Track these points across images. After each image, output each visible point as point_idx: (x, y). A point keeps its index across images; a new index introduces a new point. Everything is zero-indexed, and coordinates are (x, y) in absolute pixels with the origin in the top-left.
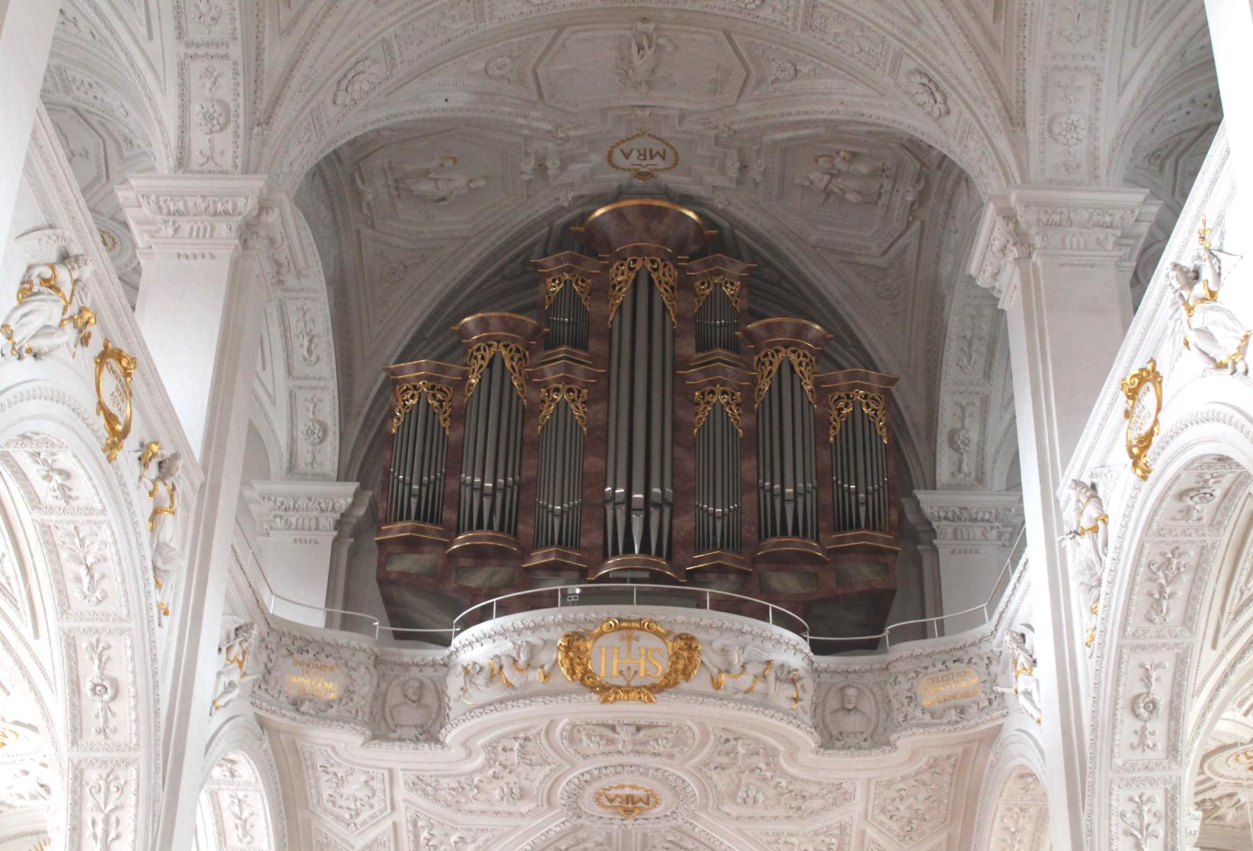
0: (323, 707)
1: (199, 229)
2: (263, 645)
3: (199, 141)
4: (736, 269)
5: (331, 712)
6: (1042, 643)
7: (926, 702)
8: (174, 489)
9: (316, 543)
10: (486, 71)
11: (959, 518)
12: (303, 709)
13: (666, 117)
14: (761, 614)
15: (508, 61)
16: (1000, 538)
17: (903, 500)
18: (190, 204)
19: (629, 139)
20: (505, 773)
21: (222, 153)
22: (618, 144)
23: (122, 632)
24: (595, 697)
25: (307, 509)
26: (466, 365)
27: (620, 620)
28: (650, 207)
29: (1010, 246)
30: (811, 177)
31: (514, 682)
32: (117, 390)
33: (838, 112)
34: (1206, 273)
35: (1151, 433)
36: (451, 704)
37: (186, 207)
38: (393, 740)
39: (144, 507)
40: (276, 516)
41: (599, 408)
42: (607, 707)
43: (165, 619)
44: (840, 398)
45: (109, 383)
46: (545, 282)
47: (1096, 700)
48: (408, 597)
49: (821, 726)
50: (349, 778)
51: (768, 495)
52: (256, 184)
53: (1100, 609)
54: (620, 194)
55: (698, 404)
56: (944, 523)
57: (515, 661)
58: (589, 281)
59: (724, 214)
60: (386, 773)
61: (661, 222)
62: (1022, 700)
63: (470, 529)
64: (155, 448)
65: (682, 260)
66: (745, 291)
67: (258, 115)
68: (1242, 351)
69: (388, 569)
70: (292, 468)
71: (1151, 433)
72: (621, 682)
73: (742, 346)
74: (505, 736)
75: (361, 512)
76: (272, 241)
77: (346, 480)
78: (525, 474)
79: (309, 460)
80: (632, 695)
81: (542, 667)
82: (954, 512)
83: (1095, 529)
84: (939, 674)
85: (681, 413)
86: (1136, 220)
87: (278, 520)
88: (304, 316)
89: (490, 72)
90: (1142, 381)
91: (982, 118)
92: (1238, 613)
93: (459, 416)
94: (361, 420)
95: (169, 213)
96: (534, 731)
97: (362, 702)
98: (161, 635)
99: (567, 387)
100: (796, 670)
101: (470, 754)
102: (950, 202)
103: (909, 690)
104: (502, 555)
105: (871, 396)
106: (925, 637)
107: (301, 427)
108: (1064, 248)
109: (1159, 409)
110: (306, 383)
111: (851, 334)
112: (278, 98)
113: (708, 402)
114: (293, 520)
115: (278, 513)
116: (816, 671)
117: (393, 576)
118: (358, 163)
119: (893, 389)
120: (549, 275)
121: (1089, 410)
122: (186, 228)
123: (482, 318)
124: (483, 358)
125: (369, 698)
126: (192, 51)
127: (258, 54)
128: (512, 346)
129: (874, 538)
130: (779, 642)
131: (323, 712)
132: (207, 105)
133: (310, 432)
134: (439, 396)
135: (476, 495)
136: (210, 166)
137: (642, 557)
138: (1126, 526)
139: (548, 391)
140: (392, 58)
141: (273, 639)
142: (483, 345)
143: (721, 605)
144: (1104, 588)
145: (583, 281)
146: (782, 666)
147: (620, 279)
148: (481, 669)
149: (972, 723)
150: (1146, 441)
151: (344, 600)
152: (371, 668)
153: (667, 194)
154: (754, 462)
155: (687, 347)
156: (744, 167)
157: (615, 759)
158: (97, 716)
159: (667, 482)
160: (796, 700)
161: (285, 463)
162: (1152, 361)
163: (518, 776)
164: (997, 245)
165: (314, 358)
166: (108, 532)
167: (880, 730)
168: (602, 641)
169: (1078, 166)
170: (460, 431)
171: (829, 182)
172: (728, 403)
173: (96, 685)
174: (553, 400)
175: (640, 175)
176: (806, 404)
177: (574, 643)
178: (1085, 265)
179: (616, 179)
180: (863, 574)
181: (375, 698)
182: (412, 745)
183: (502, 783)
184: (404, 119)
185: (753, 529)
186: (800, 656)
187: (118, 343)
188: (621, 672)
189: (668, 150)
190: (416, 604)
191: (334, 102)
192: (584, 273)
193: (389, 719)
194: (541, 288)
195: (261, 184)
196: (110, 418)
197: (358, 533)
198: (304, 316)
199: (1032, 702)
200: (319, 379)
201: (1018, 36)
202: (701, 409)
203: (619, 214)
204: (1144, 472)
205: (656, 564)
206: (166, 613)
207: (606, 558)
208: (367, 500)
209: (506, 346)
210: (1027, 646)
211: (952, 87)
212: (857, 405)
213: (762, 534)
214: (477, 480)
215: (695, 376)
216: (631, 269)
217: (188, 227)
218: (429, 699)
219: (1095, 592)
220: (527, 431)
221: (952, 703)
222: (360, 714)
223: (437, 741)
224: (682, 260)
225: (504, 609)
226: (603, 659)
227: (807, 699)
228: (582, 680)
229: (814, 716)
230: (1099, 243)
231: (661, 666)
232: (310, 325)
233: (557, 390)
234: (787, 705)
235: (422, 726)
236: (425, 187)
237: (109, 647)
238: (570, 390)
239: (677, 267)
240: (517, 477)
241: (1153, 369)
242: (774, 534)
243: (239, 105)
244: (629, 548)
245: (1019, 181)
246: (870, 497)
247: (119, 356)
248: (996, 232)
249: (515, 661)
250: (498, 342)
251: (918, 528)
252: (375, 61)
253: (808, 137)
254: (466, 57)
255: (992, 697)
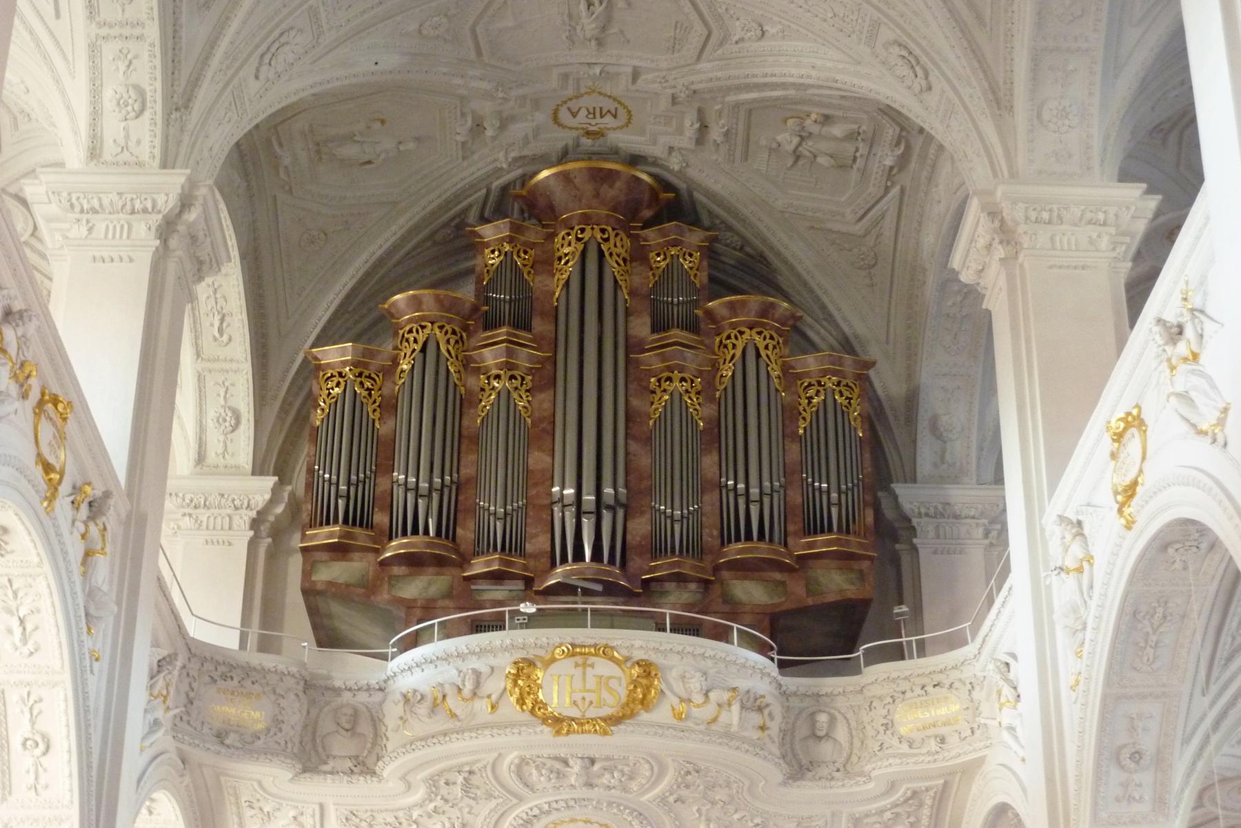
0: (249, 739)
1: (115, 227)
2: (185, 672)
3: (112, 127)
4: (695, 238)
5: (259, 743)
6: (1026, 672)
7: (903, 730)
8: (105, 529)
9: (230, 544)
10: (420, 32)
11: (942, 515)
12: (227, 742)
13: (618, 74)
14: (721, 634)
15: (444, 20)
16: (986, 535)
17: (880, 494)
18: (106, 202)
19: (577, 97)
20: (447, 808)
21: (139, 142)
22: (565, 102)
23: (55, 685)
24: (547, 729)
25: (219, 507)
26: (396, 348)
27: (574, 646)
28: (601, 170)
29: (996, 243)
30: (779, 138)
31: (458, 712)
32: (54, 437)
33: (809, 77)
34: (1189, 332)
35: (1135, 483)
36: (389, 734)
37: (101, 205)
38: (325, 773)
39: (76, 550)
40: (184, 515)
41: (544, 397)
42: (562, 739)
43: (96, 665)
44: (810, 385)
45: (46, 431)
46: (483, 253)
47: (1080, 749)
48: (336, 608)
49: (790, 756)
50: (277, 814)
51: (731, 496)
52: (176, 180)
53: (1085, 653)
54: (564, 156)
55: (653, 392)
56: (924, 520)
57: (460, 690)
58: (532, 252)
59: (681, 174)
60: (317, 808)
61: (611, 186)
62: (1006, 736)
63: (404, 534)
64: (88, 489)
65: (635, 228)
66: (705, 263)
67: (175, 99)
68: (1221, 422)
69: (313, 578)
70: (201, 459)
71: (1135, 483)
72: (575, 713)
73: (703, 326)
74: (449, 770)
75: (280, 509)
76: (193, 239)
77: (262, 473)
78: (463, 472)
79: (220, 451)
80: (586, 727)
81: (489, 696)
82: (936, 507)
83: (1080, 570)
84: (918, 700)
85: (635, 402)
86: (1133, 217)
87: (187, 518)
88: (215, 291)
89: (425, 32)
90: (1128, 426)
91: (966, 98)
92: (1229, 659)
93: (389, 407)
94: (277, 404)
95: (82, 211)
96: (480, 765)
97: (292, 733)
98: (92, 681)
99: (510, 373)
100: (763, 697)
101: (409, 786)
102: (934, 167)
103: (885, 717)
104: (440, 562)
105: (844, 383)
106: (903, 658)
107: (211, 414)
108: (1054, 249)
109: (1144, 458)
110: (217, 366)
111: (823, 307)
112: (197, 79)
113: (665, 391)
114: (205, 519)
115: (187, 511)
116: (785, 695)
117: (319, 587)
118: (275, 127)
119: (872, 373)
120: (487, 245)
121: (1079, 432)
122: (100, 227)
123: (414, 296)
124: (416, 341)
125: (298, 728)
126: (104, 31)
127: (175, 31)
128: (448, 327)
129: (848, 543)
130: (744, 666)
131: (248, 744)
132: (121, 89)
133: (220, 420)
134: (368, 384)
135: (410, 496)
136: (126, 156)
137: (595, 566)
138: (1110, 574)
139: (488, 378)
140: (320, 26)
141: (194, 666)
142: (415, 326)
143: (680, 627)
144: (1089, 634)
145: (525, 252)
146: (748, 692)
147: (566, 250)
148: (423, 697)
149: (953, 753)
150: (1130, 490)
151: (263, 609)
152: (301, 694)
153: (614, 153)
154: (716, 458)
155: (641, 327)
156: (704, 128)
157: (565, 794)
158: (28, 772)
159: (621, 481)
160: (762, 728)
161: (193, 455)
162: (1138, 406)
163: (460, 810)
164: (981, 242)
165: (225, 338)
166: (44, 584)
167: (854, 759)
168: (554, 668)
169: (1070, 156)
170: (391, 423)
171: (800, 144)
172: (687, 391)
173: (26, 740)
174: (494, 388)
175: (588, 134)
176: (772, 389)
177: (524, 668)
178: (1075, 268)
179: (559, 139)
180: (835, 583)
181: (305, 727)
182: (346, 778)
183: (444, 818)
184: (330, 86)
185: (715, 533)
186: (767, 680)
187: (55, 389)
188: (575, 703)
189: (621, 109)
190: (346, 618)
191: (257, 77)
192: (525, 244)
193: (320, 750)
194: (478, 261)
195: (182, 179)
196: (48, 468)
197: (277, 533)
198: (215, 291)
199: (1016, 738)
200: (231, 360)
201: (1006, 11)
202: (657, 398)
203: (565, 177)
204: (1128, 521)
205: (610, 573)
206: (97, 660)
207: (553, 565)
208: (286, 495)
209: (441, 328)
210: (1011, 676)
211: (935, 64)
212: (829, 394)
213: (725, 540)
214: (412, 480)
215: (651, 360)
216: (578, 239)
217: (104, 227)
218: (364, 727)
219: (1080, 635)
220: (465, 422)
221: (932, 731)
222: (289, 745)
223: (373, 773)
224: (635, 228)
225: (448, 632)
226: (556, 687)
227: (774, 727)
228: (532, 711)
229: (782, 745)
230: (1091, 241)
231: (622, 691)
232: (221, 302)
233: (498, 377)
234: (756, 735)
235: (357, 757)
236: (350, 151)
237: (41, 700)
238: (512, 377)
239: (630, 236)
240: (455, 475)
241: (1139, 416)
242: (738, 539)
243: (154, 88)
244: (579, 556)
245: (1006, 174)
246: (843, 497)
247: (55, 401)
248: (980, 230)
249: (460, 690)
250: (432, 323)
251: (897, 525)
252: (301, 31)
253: (777, 99)
254: (399, 18)
255: (975, 726)
